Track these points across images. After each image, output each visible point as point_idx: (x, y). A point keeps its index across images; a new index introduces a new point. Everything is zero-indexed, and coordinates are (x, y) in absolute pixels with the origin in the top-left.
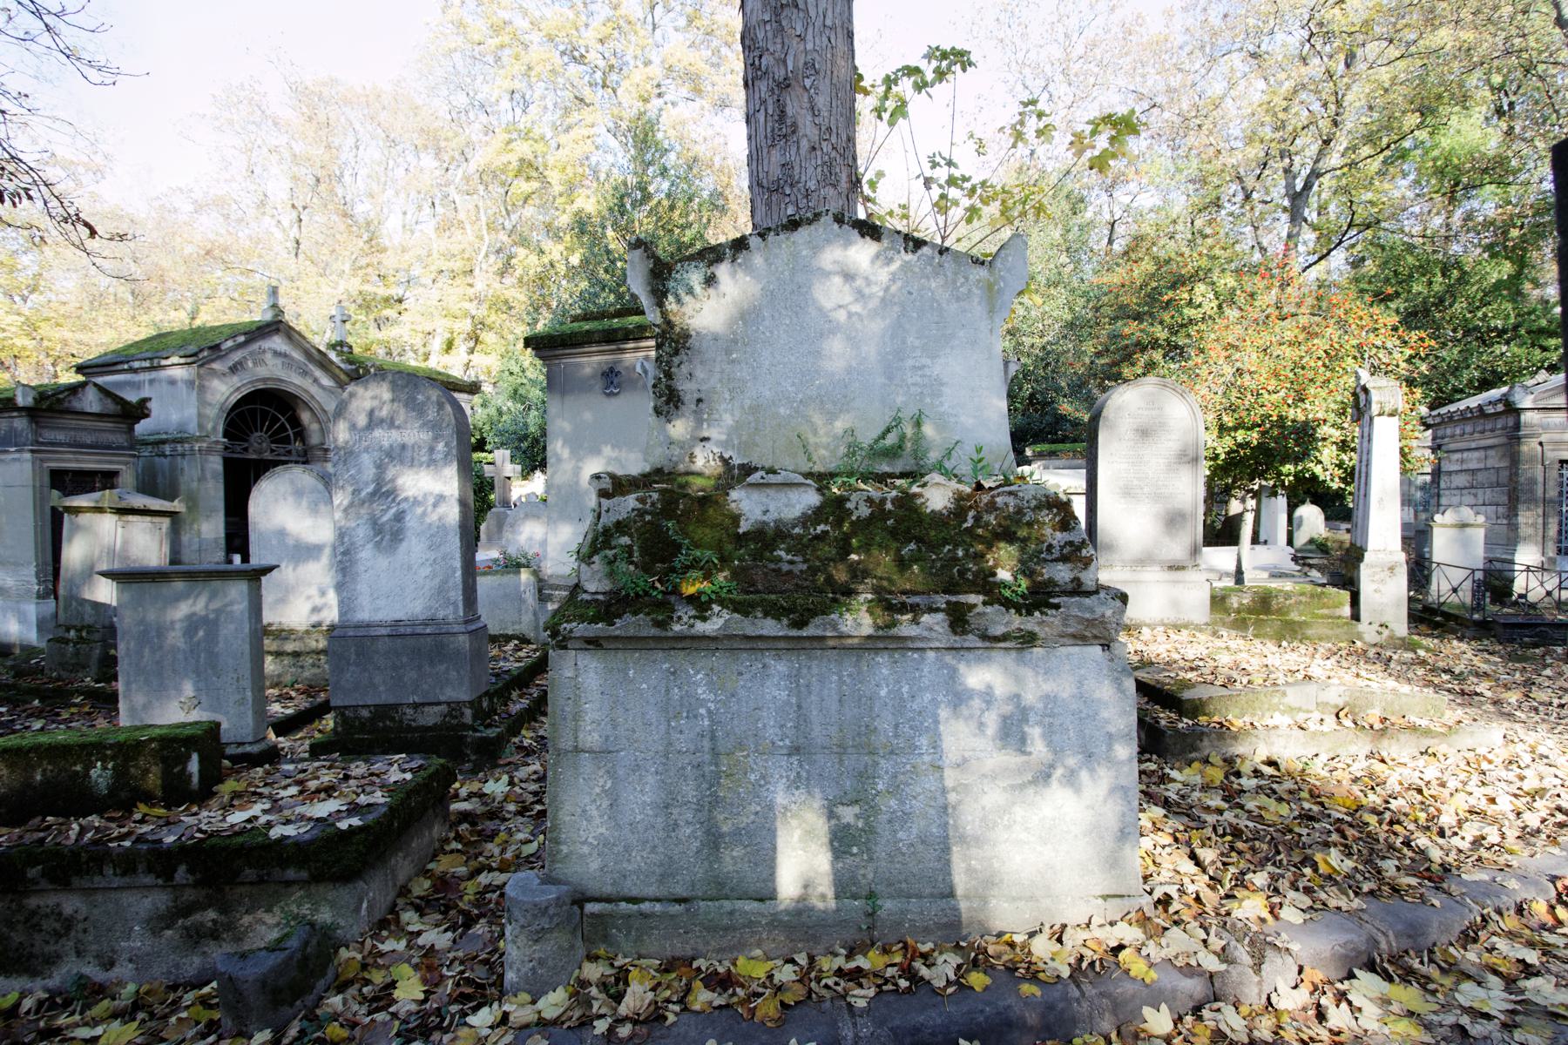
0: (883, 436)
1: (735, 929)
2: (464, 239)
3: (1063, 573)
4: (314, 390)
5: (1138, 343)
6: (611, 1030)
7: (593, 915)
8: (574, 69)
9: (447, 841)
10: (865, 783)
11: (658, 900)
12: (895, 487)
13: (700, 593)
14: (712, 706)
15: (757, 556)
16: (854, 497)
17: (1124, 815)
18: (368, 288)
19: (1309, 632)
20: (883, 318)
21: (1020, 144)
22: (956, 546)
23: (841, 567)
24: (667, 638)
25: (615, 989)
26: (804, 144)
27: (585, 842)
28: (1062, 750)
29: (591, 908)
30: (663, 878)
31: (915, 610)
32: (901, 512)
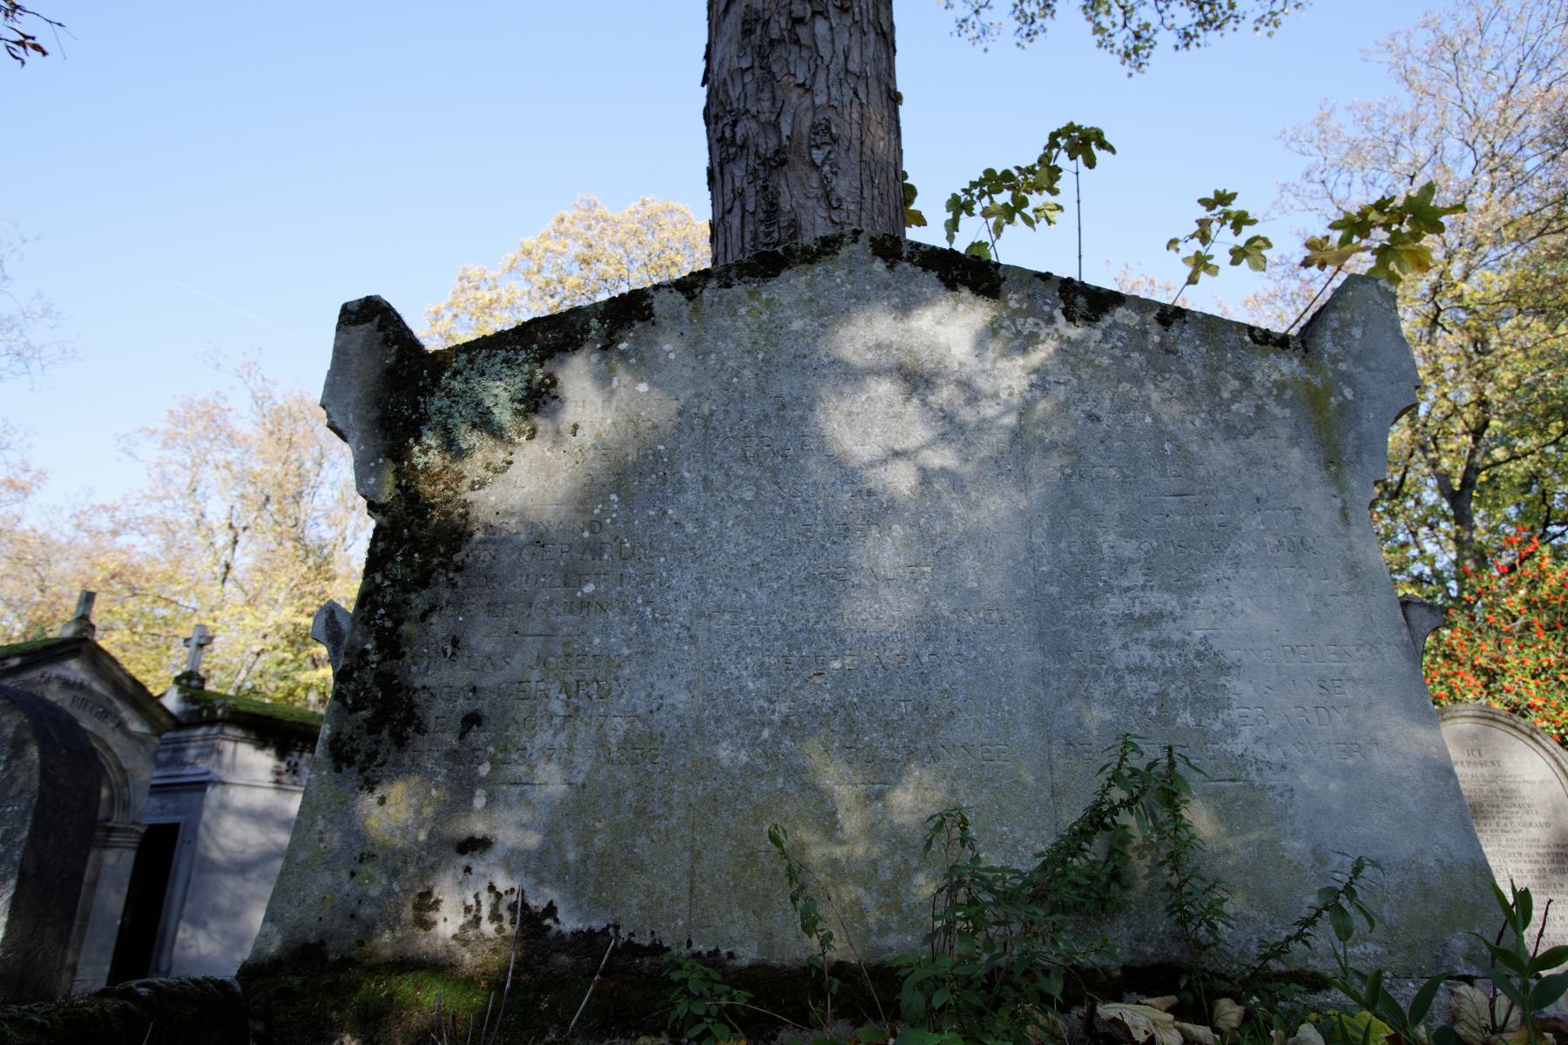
4: (114, 740)
20: (1024, 481)
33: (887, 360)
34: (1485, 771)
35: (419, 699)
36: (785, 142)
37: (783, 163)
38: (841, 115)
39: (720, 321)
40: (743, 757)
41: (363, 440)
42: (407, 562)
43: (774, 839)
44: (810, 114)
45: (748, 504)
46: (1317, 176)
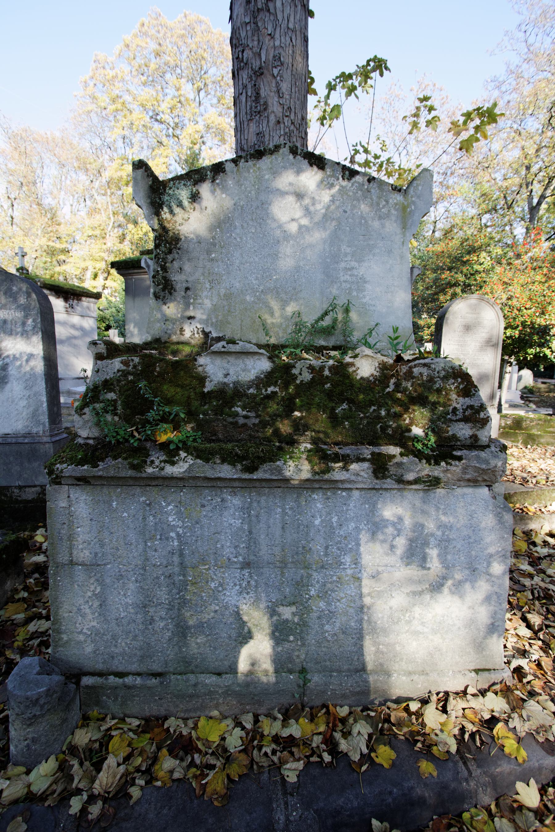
0: (322, 318)
1: (198, 697)
2: (100, 219)
3: (463, 431)
5: (449, 283)
6: (84, 811)
7: (87, 687)
8: (156, 126)
9: (16, 591)
10: (301, 585)
11: (139, 674)
12: (330, 357)
13: (169, 442)
14: (180, 531)
15: (218, 411)
16: (299, 365)
17: (495, 613)
18: (51, 244)
19: (542, 440)
20: (325, 229)
21: (415, 131)
22: (380, 407)
23: (286, 422)
24: (143, 478)
25: (96, 757)
26: (272, 118)
27: (81, 632)
28: (454, 566)
29: (87, 681)
30: (142, 659)
31: (346, 460)
32: (336, 378)
33: (291, 189)
34: (475, 316)
35: (174, 283)
36: (263, 65)
37: (262, 74)
38: (285, 51)
39: (244, 174)
40: (252, 299)
41: (147, 209)
42: (165, 247)
43: (259, 317)
44: (273, 50)
45: (253, 233)
46: (523, 28)
